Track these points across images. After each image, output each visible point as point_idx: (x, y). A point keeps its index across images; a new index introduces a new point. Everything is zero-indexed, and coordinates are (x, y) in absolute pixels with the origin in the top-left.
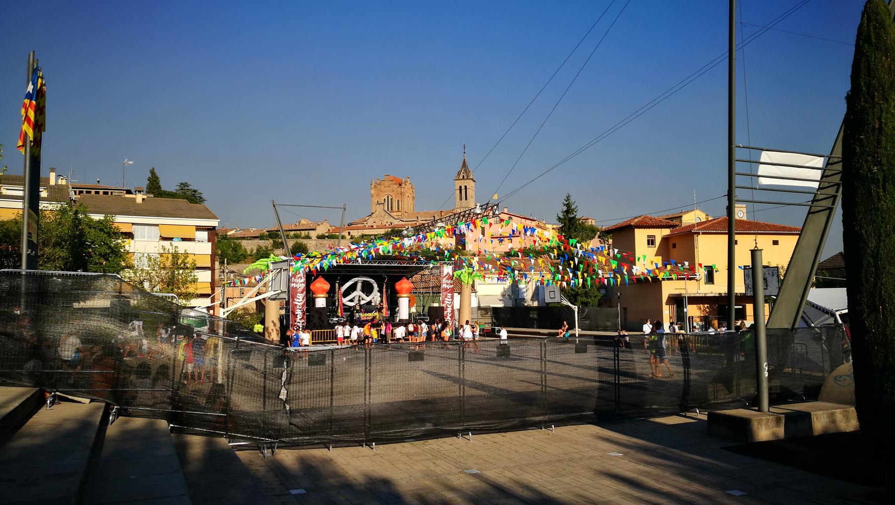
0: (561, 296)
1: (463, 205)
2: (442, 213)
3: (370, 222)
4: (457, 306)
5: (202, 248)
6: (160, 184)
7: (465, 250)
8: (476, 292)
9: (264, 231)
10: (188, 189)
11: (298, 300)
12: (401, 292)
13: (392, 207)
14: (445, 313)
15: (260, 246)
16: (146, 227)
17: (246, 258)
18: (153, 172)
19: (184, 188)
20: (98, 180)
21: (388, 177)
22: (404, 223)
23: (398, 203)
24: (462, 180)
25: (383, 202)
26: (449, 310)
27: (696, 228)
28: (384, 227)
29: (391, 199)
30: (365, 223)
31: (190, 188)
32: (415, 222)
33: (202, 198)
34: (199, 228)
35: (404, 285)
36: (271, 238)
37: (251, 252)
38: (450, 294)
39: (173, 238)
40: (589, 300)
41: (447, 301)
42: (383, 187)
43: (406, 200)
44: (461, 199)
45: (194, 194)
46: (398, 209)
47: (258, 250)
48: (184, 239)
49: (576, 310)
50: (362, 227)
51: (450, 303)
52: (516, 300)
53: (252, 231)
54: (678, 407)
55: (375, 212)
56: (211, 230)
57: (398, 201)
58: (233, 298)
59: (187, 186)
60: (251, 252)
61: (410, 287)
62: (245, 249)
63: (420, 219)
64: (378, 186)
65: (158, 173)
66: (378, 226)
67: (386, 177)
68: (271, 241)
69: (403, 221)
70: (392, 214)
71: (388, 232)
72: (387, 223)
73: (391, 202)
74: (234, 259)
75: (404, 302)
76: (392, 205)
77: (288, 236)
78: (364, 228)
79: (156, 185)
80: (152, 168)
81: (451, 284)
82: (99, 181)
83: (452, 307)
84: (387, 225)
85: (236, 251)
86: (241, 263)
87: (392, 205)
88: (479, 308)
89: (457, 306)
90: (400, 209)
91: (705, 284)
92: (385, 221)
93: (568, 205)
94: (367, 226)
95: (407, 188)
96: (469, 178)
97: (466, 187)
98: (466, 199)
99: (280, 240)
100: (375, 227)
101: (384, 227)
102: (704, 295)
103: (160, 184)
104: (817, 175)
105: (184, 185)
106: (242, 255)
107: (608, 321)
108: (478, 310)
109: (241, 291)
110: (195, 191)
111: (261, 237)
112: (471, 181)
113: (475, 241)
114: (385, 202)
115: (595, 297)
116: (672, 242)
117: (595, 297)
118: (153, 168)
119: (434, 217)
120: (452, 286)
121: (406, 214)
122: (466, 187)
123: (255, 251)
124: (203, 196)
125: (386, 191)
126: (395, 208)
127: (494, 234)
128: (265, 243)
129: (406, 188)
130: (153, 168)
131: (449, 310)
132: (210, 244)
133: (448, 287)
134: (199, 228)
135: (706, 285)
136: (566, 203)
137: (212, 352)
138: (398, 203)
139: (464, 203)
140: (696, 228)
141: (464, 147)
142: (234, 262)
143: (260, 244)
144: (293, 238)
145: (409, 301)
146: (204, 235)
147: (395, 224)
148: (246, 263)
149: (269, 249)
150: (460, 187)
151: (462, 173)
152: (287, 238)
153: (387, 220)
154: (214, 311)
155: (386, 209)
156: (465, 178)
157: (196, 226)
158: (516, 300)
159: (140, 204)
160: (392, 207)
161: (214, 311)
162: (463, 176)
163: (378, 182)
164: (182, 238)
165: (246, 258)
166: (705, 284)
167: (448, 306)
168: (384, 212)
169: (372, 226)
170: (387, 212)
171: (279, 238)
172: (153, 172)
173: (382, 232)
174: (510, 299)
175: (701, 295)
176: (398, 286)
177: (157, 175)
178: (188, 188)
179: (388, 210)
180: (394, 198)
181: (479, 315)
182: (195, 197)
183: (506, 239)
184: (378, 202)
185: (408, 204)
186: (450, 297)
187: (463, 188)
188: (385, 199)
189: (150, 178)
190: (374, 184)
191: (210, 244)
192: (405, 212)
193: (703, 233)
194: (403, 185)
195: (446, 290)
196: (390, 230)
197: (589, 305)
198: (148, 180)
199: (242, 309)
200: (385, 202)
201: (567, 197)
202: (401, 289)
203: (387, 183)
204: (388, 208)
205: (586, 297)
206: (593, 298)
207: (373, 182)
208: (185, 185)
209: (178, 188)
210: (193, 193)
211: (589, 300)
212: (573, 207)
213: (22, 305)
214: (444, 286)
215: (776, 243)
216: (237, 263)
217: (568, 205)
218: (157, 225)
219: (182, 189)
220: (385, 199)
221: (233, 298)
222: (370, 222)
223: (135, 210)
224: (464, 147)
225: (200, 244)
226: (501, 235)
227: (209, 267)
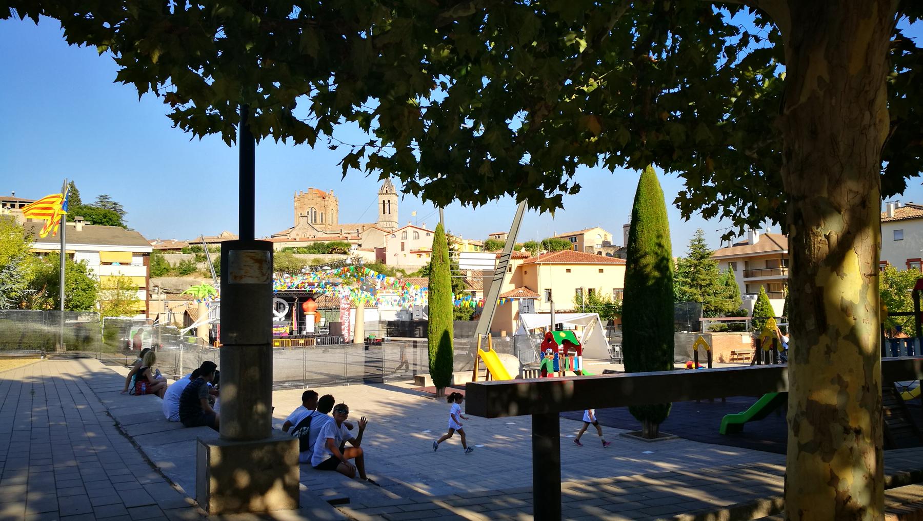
1: (387, 219)
2: (365, 228)
3: (293, 235)
4: (352, 323)
5: (138, 271)
7: (385, 264)
8: (378, 308)
9: (186, 242)
10: (108, 202)
12: (307, 310)
13: (315, 220)
14: (343, 327)
15: (183, 260)
16: (88, 253)
17: (169, 271)
19: (104, 200)
20: (13, 192)
21: (312, 190)
22: (327, 236)
23: (322, 216)
24: (385, 194)
25: (306, 215)
26: (346, 325)
27: (539, 260)
28: (308, 240)
29: (315, 212)
30: (288, 235)
31: (111, 200)
32: (339, 235)
33: (122, 210)
34: (135, 254)
35: (309, 305)
36: (194, 252)
37: (175, 266)
38: (347, 312)
39: (112, 263)
40: (463, 315)
41: (345, 317)
42: (306, 200)
43: (329, 212)
44: (384, 213)
45: (114, 207)
46: (322, 221)
47: (181, 264)
48: (121, 264)
50: (285, 239)
51: (347, 319)
53: (173, 243)
55: (299, 224)
56: (146, 255)
57: (322, 213)
59: (107, 199)
60: (175, 266)
61: (315, 307)
62: (168, 263)
63: (343, 232)
64: (302, 198)
65: (77, 187)
66: (302, 239)
67: (310, 190)
68: (194, 254)
70: (315, 226)
72: (310, 235)
73: (315, 215)
74: (157, 272)
75: (310, 320)
76: (315, 217)
77: (210, 250)
78: (287, 241)
79: (76, 199)
81: (348, 304)
82: (14, 193)
83: (349, 322)
84: (310, 238)
85: (159, 264)
86: (165, 276)
87: (315, 217)
88: (381, 322)
89: (352, 323)
90: (324, 221)
92: (308, 234)
94: (290, 239)
95: (330, 202)
96: (392, 192)
97: (389, 201)
98: (389, 213)
99: (203, 254)
100: (298, 240)
101: (308, 240)
104: (493, 262)
106: (164, 268)
107: (470, 331)
108: (379, 323)
109: (165, 304)
110: (115, 204)
111: (184, 251)
112: (394, 195)
113: (395, 255)
114: (308, 214)
115: (468, 312)
116: (524, 269)
117: (468, 312)
119: (358, 230)
120: (349, 305)
121: (330, 227)
122: (389, 201)
123: (178, 265)
124: (124, 209)
125: (309, 204)
126: (319, 220)
127: (413, 249)
128: (187, 256)
129: (330, 201)
131: (346, 325)
132: (145, 267)
133: (346, 306)
134: (135, 254)
138: (322, 216)
140: (539, 260)
142: (157, 275)
143: (183, 258)
144: (215, 252)
145: (315, 317)
146: (140, 260)
147: (318, 236)
148: (169, 276)
149: (192, 263)
150: (384, 201)
151: (385, 187)
152: (209, 252)
153: (311, 233)
155: (310, 222)
156: (388, 192)
160: (315, 220)
162: (387, 191)
163: (302, 194)
164: (120, 263)
165: (169, 271)
167: (345, 321)
168: (308, 225)
169: (295, 239)
170: (311, 224)
171: (202, 252)
173: (305, 244)
176: (305, 306)
177: (76, 188)
179: (312, 222)
180: (317, 211)
181: (381, 327)
182: (115, 210)
183: (424, 254)
184: (301, 214)
185: (331, 217)
186: (347, 314)
187: (386, 202)
188: (308, 212)
190: (298, 197)
191: (145, 267)
192: (329, 225)
193: (543, 264)
194: (327, 198)
195: (344, 309)
196: (312, 243)
197: (462, 319)
200: (308, 214)
202: (308, 308)
203: (310, 196)
204: (312, 220)
205: (461, 312)
206: (466, 313)
207: (297, 194)
208: (105, 197)
209: (97, 200)
210: (114, 205)
211: (463, 315)
213: (79, 327)
214: (342, 306)
215: (601, 271)
216: (161, 276)
218: (98, 252)
219: (102, 202)
220: (308, 212)
222: (293, 235)
223: (77, 238)
225: (136, 267)
226: (419, 250)
227: (144, 288)
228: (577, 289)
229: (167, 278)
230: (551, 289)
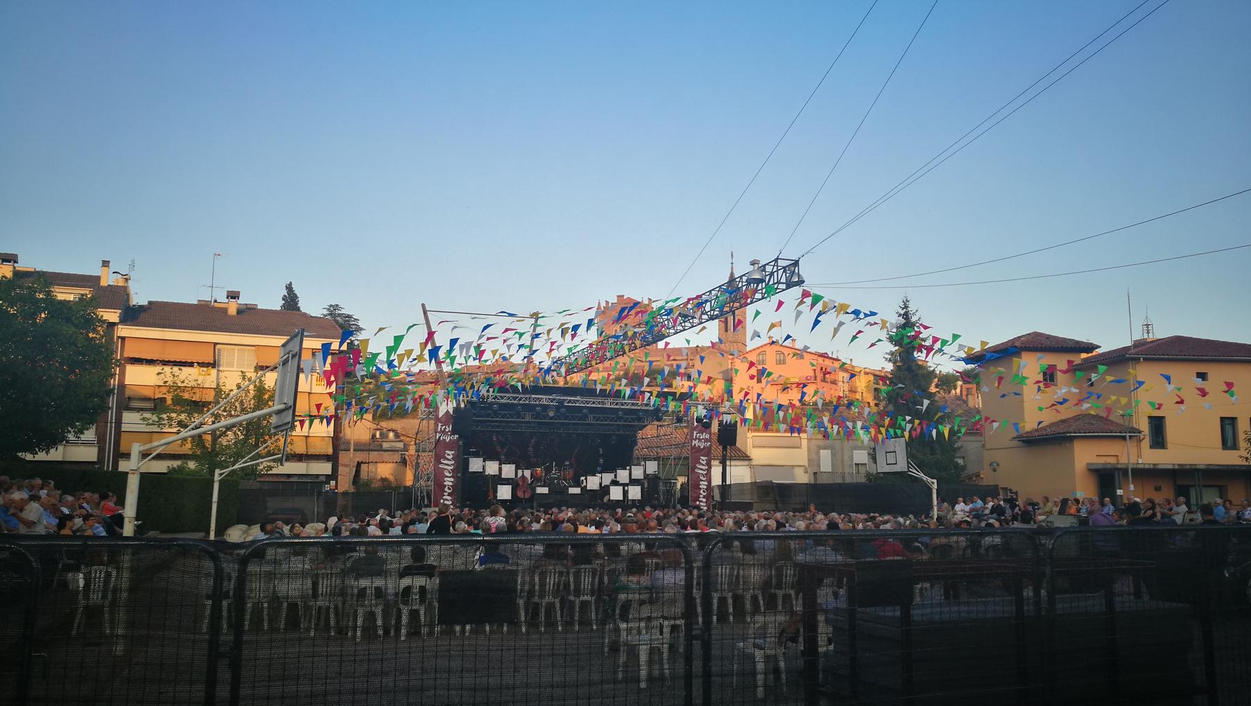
0: (908, 463)
6: (299, 305)
11: (446, 462)
18: (289, 288)
31: (343, 311)
49: (935, 486)
52: (815, 473)
54: (139, 378)
58: (369, 462)
69: (642, 362)
71: (619, 375)
80: (289, 283)
91: (1151, 447)
93: (906, 316)
102: (1152, 467)
103: (299, 305)
105: (333, 309)
110: (349, 316)
118: (291, 283)
130: (291, 283)
135: (1169, 445)
136: (902, 312)
137: (351, 546)
139: (731, 336)
141: (732, 256)
154: (337, 483)
157: (313, 349)
158: (815, 473)
159: (233, 316)
161: (337, 483)
166: (1151, 447)
172: (289, 288)
174: (806, 472)
175: (1147, 466)
178: (339, 312)
186: (704, 463)
189: (285, 296)
198: (283, 299)
199: (379, 480)
201: (904, 302)
208: (336, 307)
209: (326, 312)
212: (914, 319)
217: (906, 316)
221: (369, 462)
224: (732, 256)
228: (1222, 419)
229: (411, 420)
230: (1222, 419)
